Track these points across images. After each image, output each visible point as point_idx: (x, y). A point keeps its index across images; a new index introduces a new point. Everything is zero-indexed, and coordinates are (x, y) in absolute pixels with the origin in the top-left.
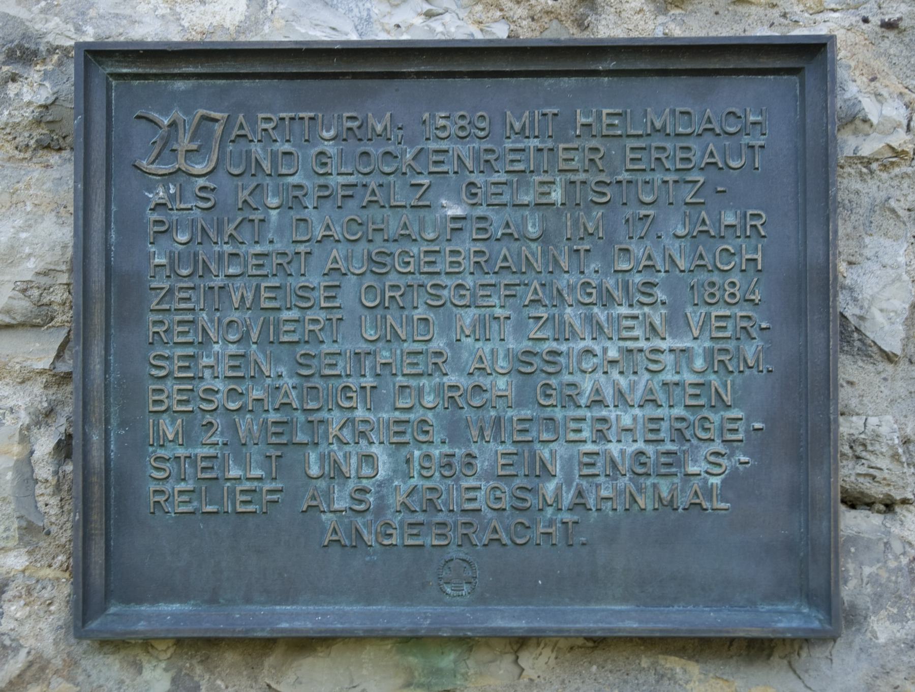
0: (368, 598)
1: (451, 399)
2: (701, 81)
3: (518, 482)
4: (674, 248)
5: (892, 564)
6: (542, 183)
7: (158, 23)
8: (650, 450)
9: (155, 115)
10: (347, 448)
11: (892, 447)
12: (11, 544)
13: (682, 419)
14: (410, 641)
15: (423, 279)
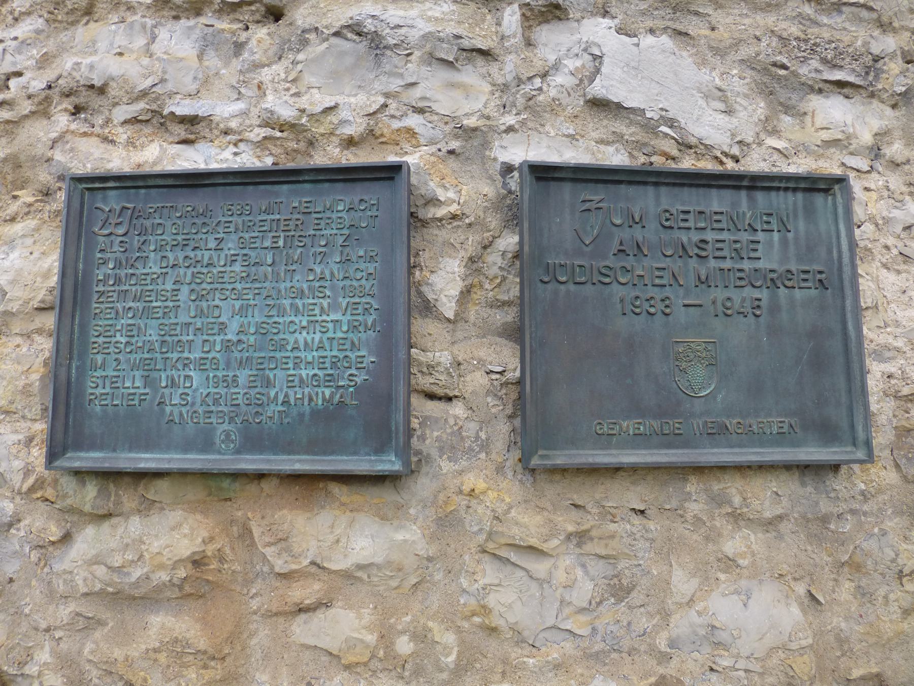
0: (186, 450)
1: (228, 346)
2: (348, 184)
3: (257, 390)
4: (335, 268)
5: (449, 431)
6: (274, 237)
7: (120, 161)
8: (321, 373)
9: (103, 206)
10: (179, 373)
11: (447, 369)
12: (38, 417)
13: (336, 357)
14: (205, 475)
15: (218, 286)
